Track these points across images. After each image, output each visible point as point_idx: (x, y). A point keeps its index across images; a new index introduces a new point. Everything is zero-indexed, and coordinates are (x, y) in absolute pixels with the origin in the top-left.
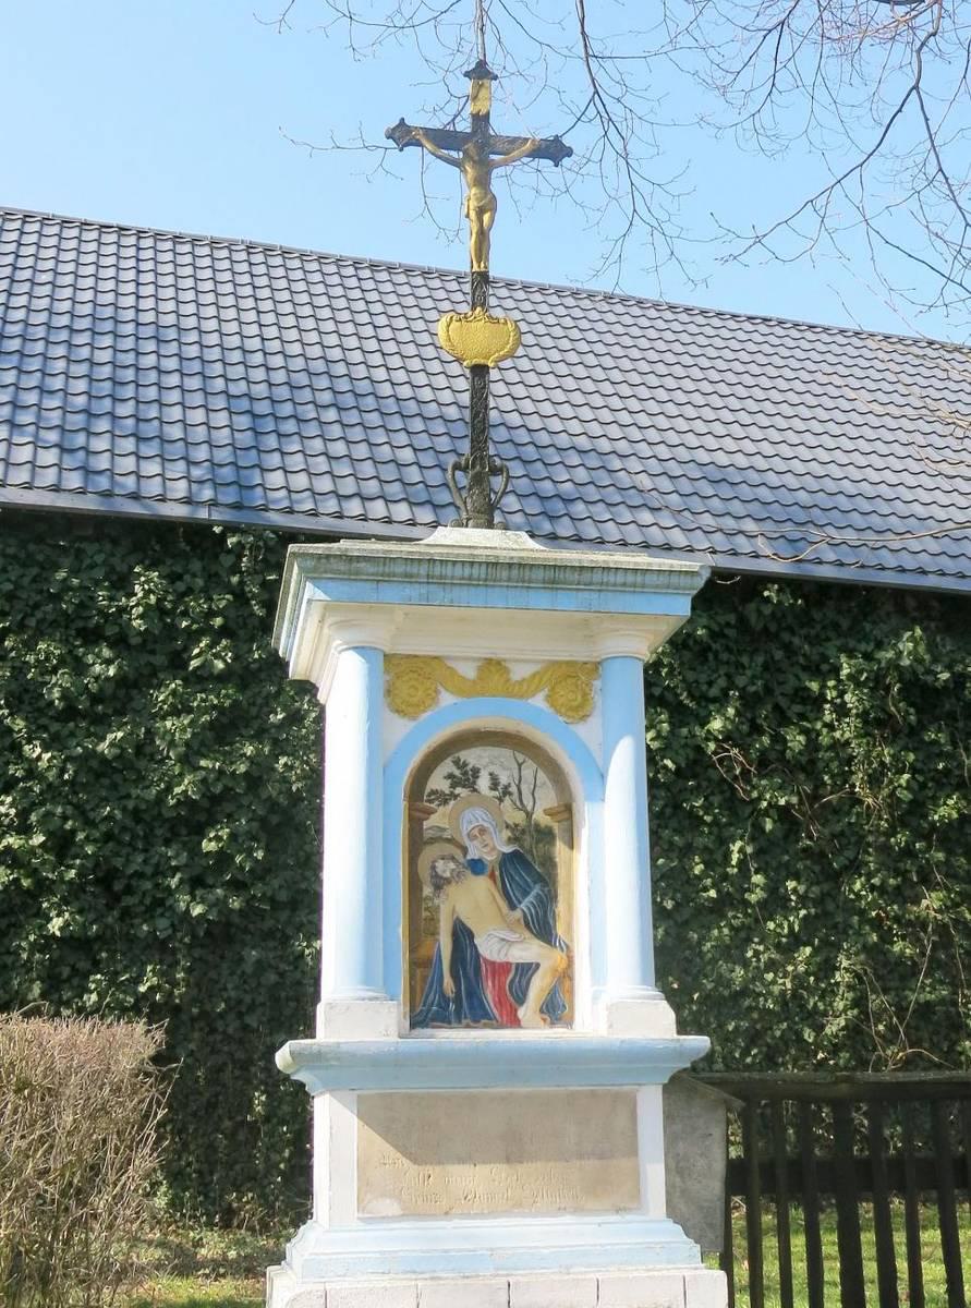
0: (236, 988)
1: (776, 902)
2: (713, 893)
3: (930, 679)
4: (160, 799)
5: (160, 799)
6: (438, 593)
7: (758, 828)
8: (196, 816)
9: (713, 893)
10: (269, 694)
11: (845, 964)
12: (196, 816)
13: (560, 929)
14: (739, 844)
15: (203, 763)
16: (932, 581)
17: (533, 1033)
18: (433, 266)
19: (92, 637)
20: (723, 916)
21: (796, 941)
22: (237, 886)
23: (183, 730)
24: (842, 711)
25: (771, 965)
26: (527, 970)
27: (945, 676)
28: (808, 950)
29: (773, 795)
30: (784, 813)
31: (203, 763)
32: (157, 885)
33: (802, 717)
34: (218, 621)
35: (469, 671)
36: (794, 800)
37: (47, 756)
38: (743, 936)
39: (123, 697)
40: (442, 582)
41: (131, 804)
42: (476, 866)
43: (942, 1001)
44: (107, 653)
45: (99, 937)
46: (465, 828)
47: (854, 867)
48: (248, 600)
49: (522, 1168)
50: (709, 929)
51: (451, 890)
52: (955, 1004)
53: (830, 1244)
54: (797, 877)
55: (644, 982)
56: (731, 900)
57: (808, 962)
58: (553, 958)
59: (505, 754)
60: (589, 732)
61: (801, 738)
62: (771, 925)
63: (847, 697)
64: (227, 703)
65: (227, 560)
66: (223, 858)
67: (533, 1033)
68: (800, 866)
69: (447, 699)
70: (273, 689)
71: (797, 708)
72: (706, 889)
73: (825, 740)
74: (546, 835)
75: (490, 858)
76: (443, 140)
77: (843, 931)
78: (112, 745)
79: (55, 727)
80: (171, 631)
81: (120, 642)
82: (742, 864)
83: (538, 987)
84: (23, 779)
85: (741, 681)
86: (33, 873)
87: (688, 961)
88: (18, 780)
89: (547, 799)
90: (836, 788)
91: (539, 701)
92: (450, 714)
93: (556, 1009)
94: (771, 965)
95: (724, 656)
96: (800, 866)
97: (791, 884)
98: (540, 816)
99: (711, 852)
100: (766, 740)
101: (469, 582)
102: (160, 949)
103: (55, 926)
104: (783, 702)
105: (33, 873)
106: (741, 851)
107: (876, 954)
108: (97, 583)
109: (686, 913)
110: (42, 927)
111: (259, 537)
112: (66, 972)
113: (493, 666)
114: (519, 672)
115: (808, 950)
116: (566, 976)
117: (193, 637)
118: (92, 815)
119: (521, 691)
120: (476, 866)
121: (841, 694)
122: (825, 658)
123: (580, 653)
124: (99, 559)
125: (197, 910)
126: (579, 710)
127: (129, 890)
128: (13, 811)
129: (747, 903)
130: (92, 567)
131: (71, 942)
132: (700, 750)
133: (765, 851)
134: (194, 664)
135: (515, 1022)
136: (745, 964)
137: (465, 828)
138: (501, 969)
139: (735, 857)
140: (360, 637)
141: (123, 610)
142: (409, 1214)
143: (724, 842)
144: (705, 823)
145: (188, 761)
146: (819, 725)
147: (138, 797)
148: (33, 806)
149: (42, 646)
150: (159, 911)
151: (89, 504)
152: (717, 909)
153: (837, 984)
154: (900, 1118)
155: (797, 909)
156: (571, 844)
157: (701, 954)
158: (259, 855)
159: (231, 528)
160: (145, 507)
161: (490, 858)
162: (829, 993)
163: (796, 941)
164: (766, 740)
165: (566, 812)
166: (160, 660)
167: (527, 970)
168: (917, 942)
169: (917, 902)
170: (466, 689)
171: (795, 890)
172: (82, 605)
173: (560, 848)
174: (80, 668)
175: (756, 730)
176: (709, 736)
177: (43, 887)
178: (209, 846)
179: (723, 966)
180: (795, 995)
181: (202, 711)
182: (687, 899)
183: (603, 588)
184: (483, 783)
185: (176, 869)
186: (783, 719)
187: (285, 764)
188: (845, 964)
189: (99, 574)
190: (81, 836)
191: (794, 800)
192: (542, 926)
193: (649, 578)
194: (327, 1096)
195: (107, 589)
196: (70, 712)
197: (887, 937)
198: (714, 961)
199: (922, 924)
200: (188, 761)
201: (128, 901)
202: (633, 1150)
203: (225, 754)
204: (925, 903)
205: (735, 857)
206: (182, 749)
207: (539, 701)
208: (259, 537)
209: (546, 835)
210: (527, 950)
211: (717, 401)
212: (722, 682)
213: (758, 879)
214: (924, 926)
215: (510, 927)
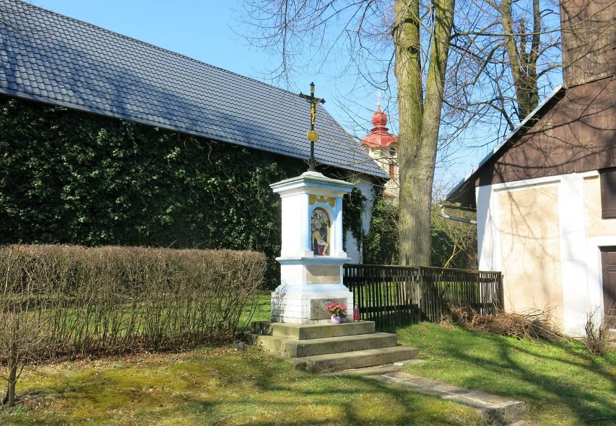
0: (122, 237)
1: (239, 223)
2: (226, 220)
3: (274, 174)
4: (106, 190)
5: (106, 190)
6: (321, 186)
7: (237, 206)
8: (114, 194)
9: (226, 220)
10: (131, 164)
11: (252, 237)
12: (114, 194)
13: (328, 240)
14: (232, 209)
15: (117, 181)
16: (276, 151)
17: (324, 256)
18: (149, 43)
19: (87, 145)
20: (227, 225)
21: (242, 232)
22: (124, 212)
23: (112, 172)
24: (256, 180)
25: (236, 237)
26: (324, 246)
27: (277, 174)
28: (244, 234)
29: (239, 198)
30: (242, 202)
31: (117, 181)
32: (105, 211)
33: (246, 180)
34: (119, 144)
35: (319, 198)
36: (245, 200)
37: (79, 176)
38: (231, 230)
39: (94, 163)
40: (321, 184)
41: (99, 190)
42: (317, 229)
43: (269, 247)
44: (91, 150)
45: (91, 223)
46: (316, 223)
47: (254, 216)
48: (132, 141)
49: (327, 277)
50: (224, 228)
51: (314, 233)
52: (272, 247)
53: (371, 287)
54: (243, 217)
55: (309, 248)
56: (230, 222)
57: (244, 237)
58: (327, 245)
59: (321, 211)
60: (334, 209)
61: (247, 185)
62: (237, 228)
63: (257, 177)
64: (121, 166)
65: (122, 128)
66: (121, 205)
67: (324, 256)
68: (244, 215)
69: (316, 202)
70: (132, 163)
71: (245, 178)
72: (224, 219)
73: (251, 186)
74: (326, 225)
75: (319, 228)
76: (307, 97)
77: (251, 230)
78: (95, 174)
79: (79, 168)
80: (108, 145)
81: (95, 147)
82: (232, 213)
83: (325, 249)
84: (73, 182)
85: (235, 170)
86: (75, 206)
87: (220, 235)
88: (71, 182)
89: (326, 219)
90: (252, 198)
91: (328, 203)
92: (317, 204)
93: (327, 253)
94: (236, 237)
95: (231, 164)
96: (244, 215)
97: (242, 219)
98: (325, 222)
99: (226, 210)
100: (240, 185)
101: (325, 184)
102: (106, 227)
103: (81, 220)
104: (242, 176)
105: (75, 206)
106: (233, 210)
107: (258, 236)
108: (89, 131)
109: (220, 224)
110: (77, 220)
111: (132, 124)
112: (82, 231)
113: (322, 197)
114: (325, 198)
115: (244, 234)
116: (329, 248)
117: (113, 148)
118: (90, 192)
119: (326, 202)
120: (317, 229)
121: (256, 176)
122: (252, 167)
123: (333, 196)
124: (89, 124)
125: (116, 218)
126: (333, 206)
127: (98, 211)
128: (70, 190)
129: (233, 223)
130: (87, 126)
131: (85, 224)
132: (226, 186)
133: (238, 210)
134: (114, 155)
135: (322, 255)
136: (231, 236)
137: (316, 223)
138: (320, 246)
139: (231, 212)
140: (308, 192)
141: (96, 139)
142: (312, 283)
143: (229, 208)
144: (225, 203)
145: (113, 180)
146: (250, 182)
147: (101, 188)
148: (76, 189)
149: (75, 146)
150: (105, 217)
151: (87, 109)
152: (225, 224)
153: (250, 242)
154: (370, 270)
155: (243, 225)
156: (330, 227)
157: (222, 234)
158: (130, 205)
159: (124, 120)
160: (102, 112)
161: (319, 228)
162: (248, 243)
163: (242, 232)
164: (240, 185)
165: (329, 222)
166: (104, 153)
167: (324, 246)
168: (265, 233)
169: (266, 225)
170: (319, 201)
171: (243, 220)
172: (85, 137)
173: (328, 227)
174: (85, 153)
175: (238, 183)
176: (228, 183)
177: (77, 210)
178: (118, 202)
179: (227, 237)
180: (242, 245)
181: (116, 167)
182: (220, 221)
183: (342, 187)
184: (318, 216)
185: (110, 207)
186: (242, 180)
187: (134, 183)
188: (252, 237)
189: (89, 128)
190: (88, 197)
191: (245, 200)
192: (325, 240)
193: (348, 186)
194: (302, 265)
195: (91, 133)
196: (83, 165)
197: (260, 232)
198: (225, 235)
199: (267, 230)
200: (113, 180)
201: (98, 214)
202: (339, 275)
203: (121, 179)
204: (268, 225)
205: (231, 212)
206: (111, 177)
207: (328, 203)
208: (132, 124)
209: (326, 225)
210: (323, 243)
211: (95, 42)
212: (231, 170)
213: (235, 217)
214: (268, 230)
215: (321, 239)
